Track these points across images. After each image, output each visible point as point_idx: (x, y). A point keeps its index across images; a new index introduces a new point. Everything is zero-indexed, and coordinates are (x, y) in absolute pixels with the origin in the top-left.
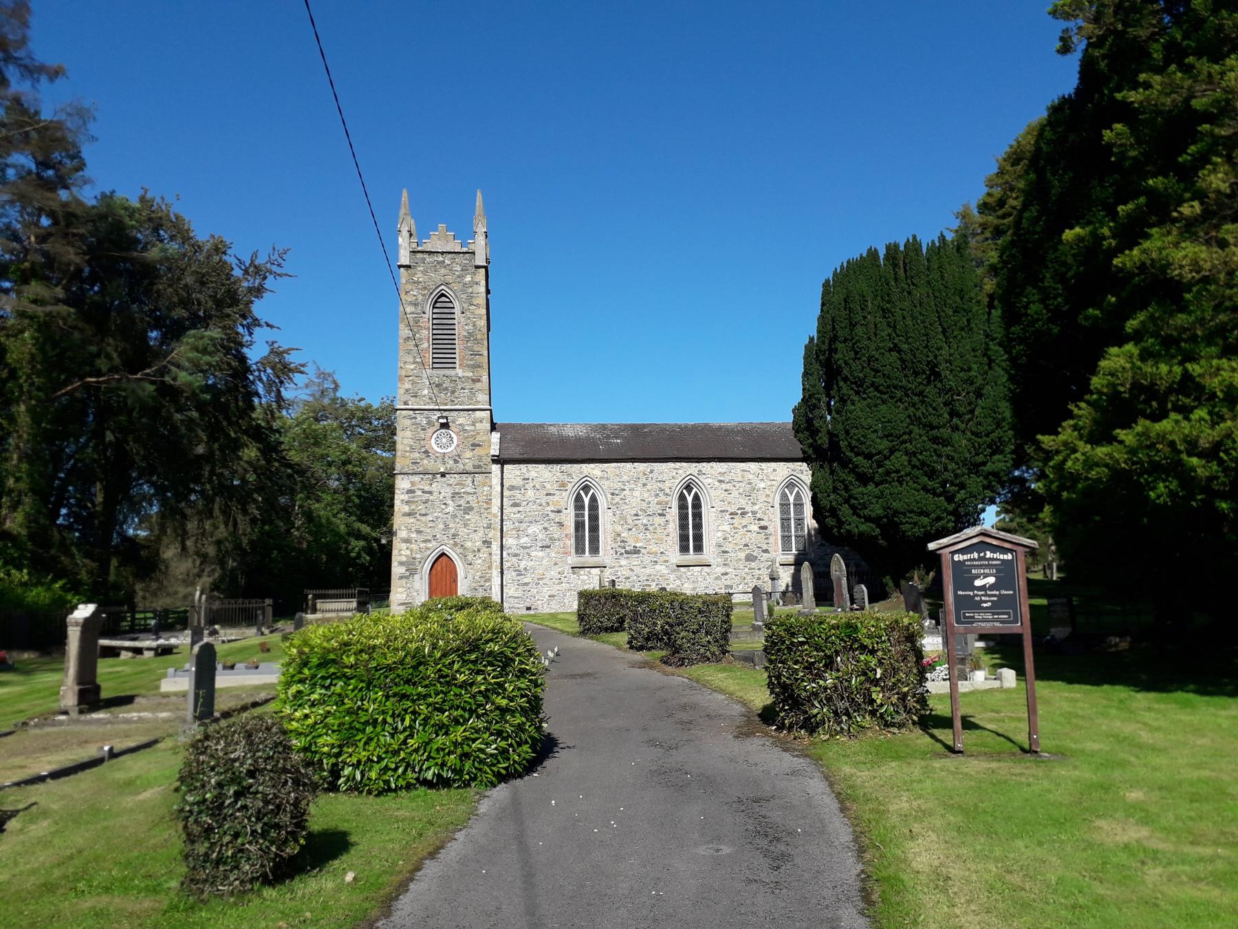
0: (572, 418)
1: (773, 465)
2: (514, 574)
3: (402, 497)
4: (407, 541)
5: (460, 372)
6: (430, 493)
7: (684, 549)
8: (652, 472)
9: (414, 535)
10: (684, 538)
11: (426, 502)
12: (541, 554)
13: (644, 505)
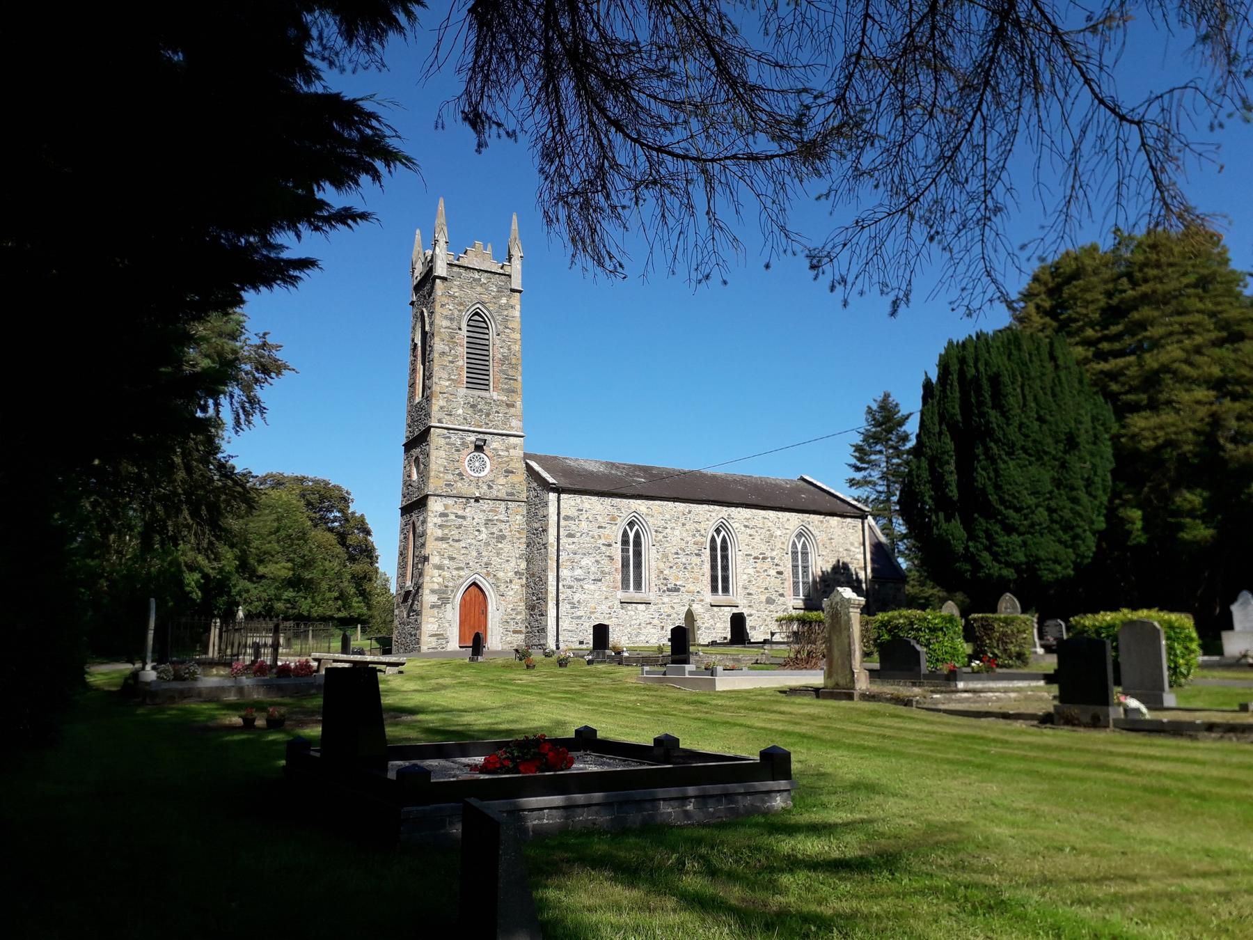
0: (590, 456)
1: (787, 514)
2: (568, 606)
3: (435, 520)
4: (439, 567)
5: (495, 395)
6: (464, 518)
7: (714, 589)
8: (690, 512)
9: (446, 562)
10: (714, 579)
11: (460, 527)
12: (593, 587)
13: (683, 545)
